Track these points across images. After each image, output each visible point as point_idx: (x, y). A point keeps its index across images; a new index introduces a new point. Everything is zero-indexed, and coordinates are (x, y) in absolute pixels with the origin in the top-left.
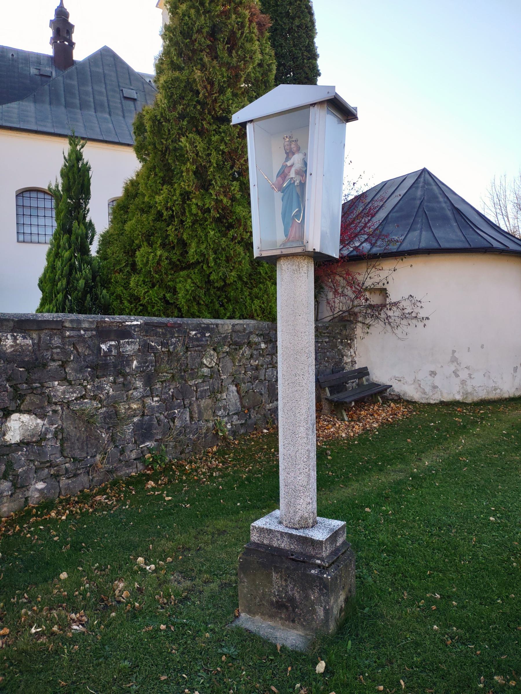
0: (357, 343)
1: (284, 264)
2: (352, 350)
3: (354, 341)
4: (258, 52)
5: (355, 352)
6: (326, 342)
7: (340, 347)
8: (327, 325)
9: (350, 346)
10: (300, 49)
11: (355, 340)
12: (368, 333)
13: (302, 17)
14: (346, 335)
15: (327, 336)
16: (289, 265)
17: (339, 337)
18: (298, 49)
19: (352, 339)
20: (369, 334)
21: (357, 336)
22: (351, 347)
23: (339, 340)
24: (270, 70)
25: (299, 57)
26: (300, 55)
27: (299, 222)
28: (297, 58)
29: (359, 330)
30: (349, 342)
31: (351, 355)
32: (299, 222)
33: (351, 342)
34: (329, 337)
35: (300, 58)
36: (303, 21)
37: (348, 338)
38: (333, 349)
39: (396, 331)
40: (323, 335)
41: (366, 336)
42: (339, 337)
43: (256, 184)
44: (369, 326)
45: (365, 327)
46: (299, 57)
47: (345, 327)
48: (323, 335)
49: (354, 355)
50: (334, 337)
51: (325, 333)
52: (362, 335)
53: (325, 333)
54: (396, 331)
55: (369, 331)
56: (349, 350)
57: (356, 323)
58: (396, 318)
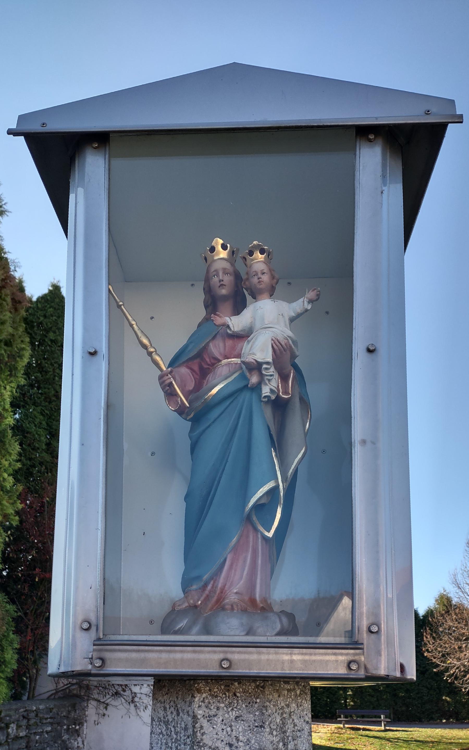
0: (88, 730)
1: (210, 718)
2: (79, 739)
3: (83, 725)
4: (8, 324)
5: (83, 744)
6: (47, 732)
7: (66, 737)
8: (52, 706)
9: (77, 733)
10: (52, 364)
11: (85, 724)
12: (104, 715)
13: (58, 333)
14: (74, 718)
15: (49, 723)
16: (240, 727)
17: (65, 722)
18: (49, 363)
19: (81, 724)
20: (106, 716)
21: (87, 718)
22: (78, 736)
23: (65, 727)
24: (21, 357)
25: (49, 372)
26: (51, 370)
27: (270, 534)
28: (46, 372)
29: (91, 710)
30: (77, 727)
31: (78, 747)
32: (270, 534)
33: (80, 728)
34: (51, 724)
35: (50, 373)
36: (59, 338)
37: (77, 722)
38: (55, 742)
39: (142, 713)
40: (44, 721)
41: (101, 720)
42: (65, 722)
43: (103, 349)
44: (107, 706)
45: (102, 707)
46: (49, 372)
47: (74, 707)
48: (44, 721)
49: (82, 746)
50: (58, 724)
51: (47, 719)
52: (95, 718)
53: (47, 719)
54: (142, 713)
55: (105, 712)
56: (75, 740)
57: (88, 700)
58: (143, 697)
